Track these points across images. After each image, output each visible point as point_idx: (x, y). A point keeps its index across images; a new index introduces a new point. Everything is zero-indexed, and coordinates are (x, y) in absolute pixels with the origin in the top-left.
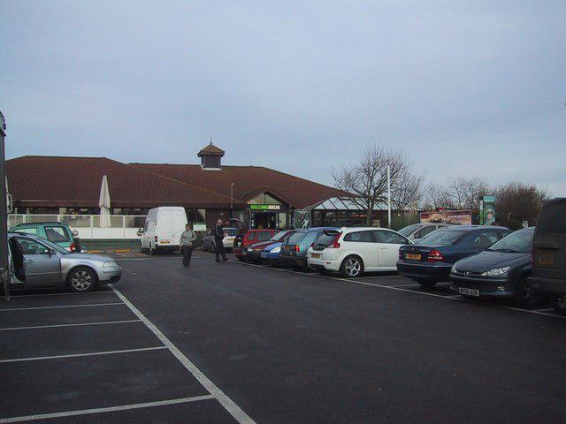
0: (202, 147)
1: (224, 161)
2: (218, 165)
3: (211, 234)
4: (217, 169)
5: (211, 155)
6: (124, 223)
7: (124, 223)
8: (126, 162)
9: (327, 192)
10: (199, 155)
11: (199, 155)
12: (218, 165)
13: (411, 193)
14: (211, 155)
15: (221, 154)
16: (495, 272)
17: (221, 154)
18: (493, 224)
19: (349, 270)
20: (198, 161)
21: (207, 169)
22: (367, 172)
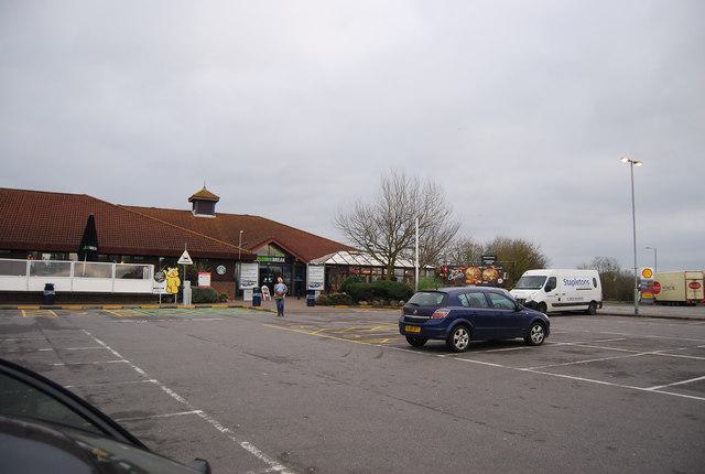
0: (195, 190)
1: (218, 208)
2: (211, 211)
3: (429, 256)
4: (210, 216)
5: (204, 202)
6: (114, 275)
7: (114, 275)
8: (115, 203)
9: (336, 247)
10: (192, 200)
11: (192, 200)
12: (211, 211)
13: (480, 249)
14: (204, 202)
15: (214, 200)
16: (80, 443)
17: (214, 200)
18: (417, 315)
19: (456, 341)
20: (189, 206)
21: (200, 215)
22: (389, 224)
